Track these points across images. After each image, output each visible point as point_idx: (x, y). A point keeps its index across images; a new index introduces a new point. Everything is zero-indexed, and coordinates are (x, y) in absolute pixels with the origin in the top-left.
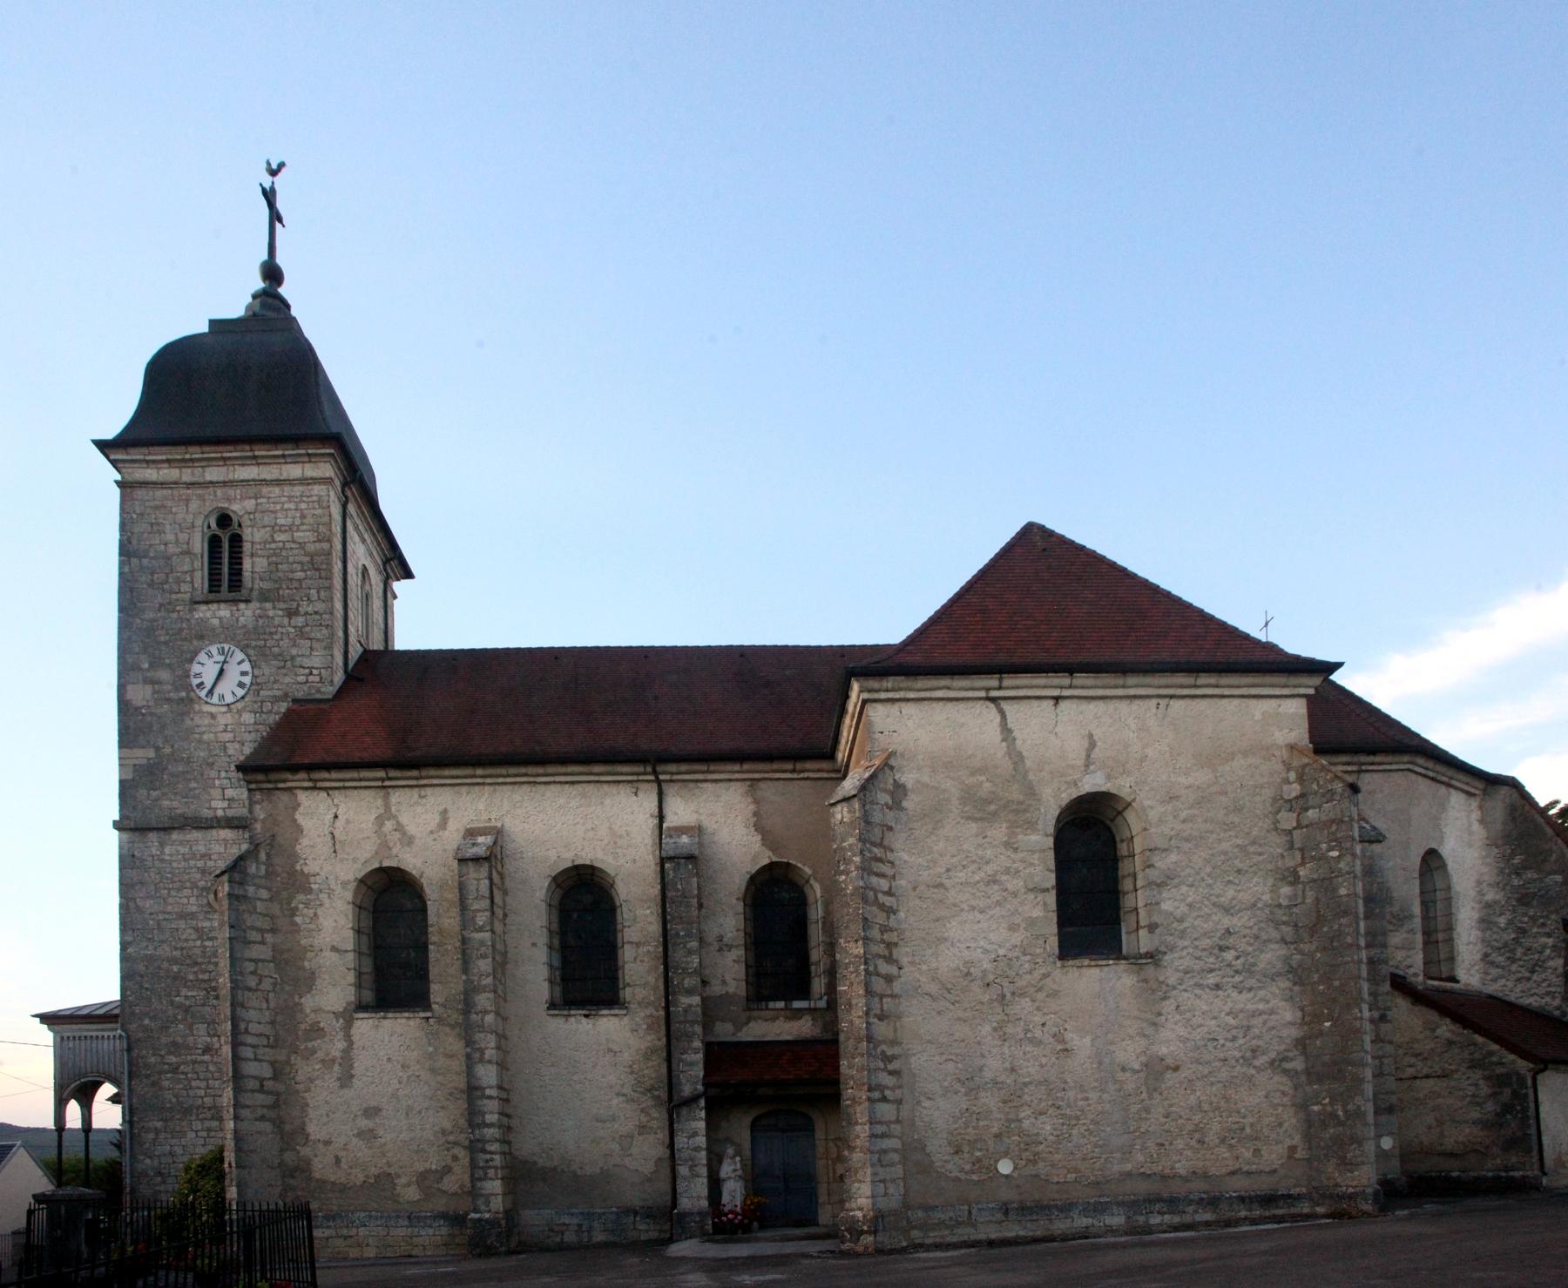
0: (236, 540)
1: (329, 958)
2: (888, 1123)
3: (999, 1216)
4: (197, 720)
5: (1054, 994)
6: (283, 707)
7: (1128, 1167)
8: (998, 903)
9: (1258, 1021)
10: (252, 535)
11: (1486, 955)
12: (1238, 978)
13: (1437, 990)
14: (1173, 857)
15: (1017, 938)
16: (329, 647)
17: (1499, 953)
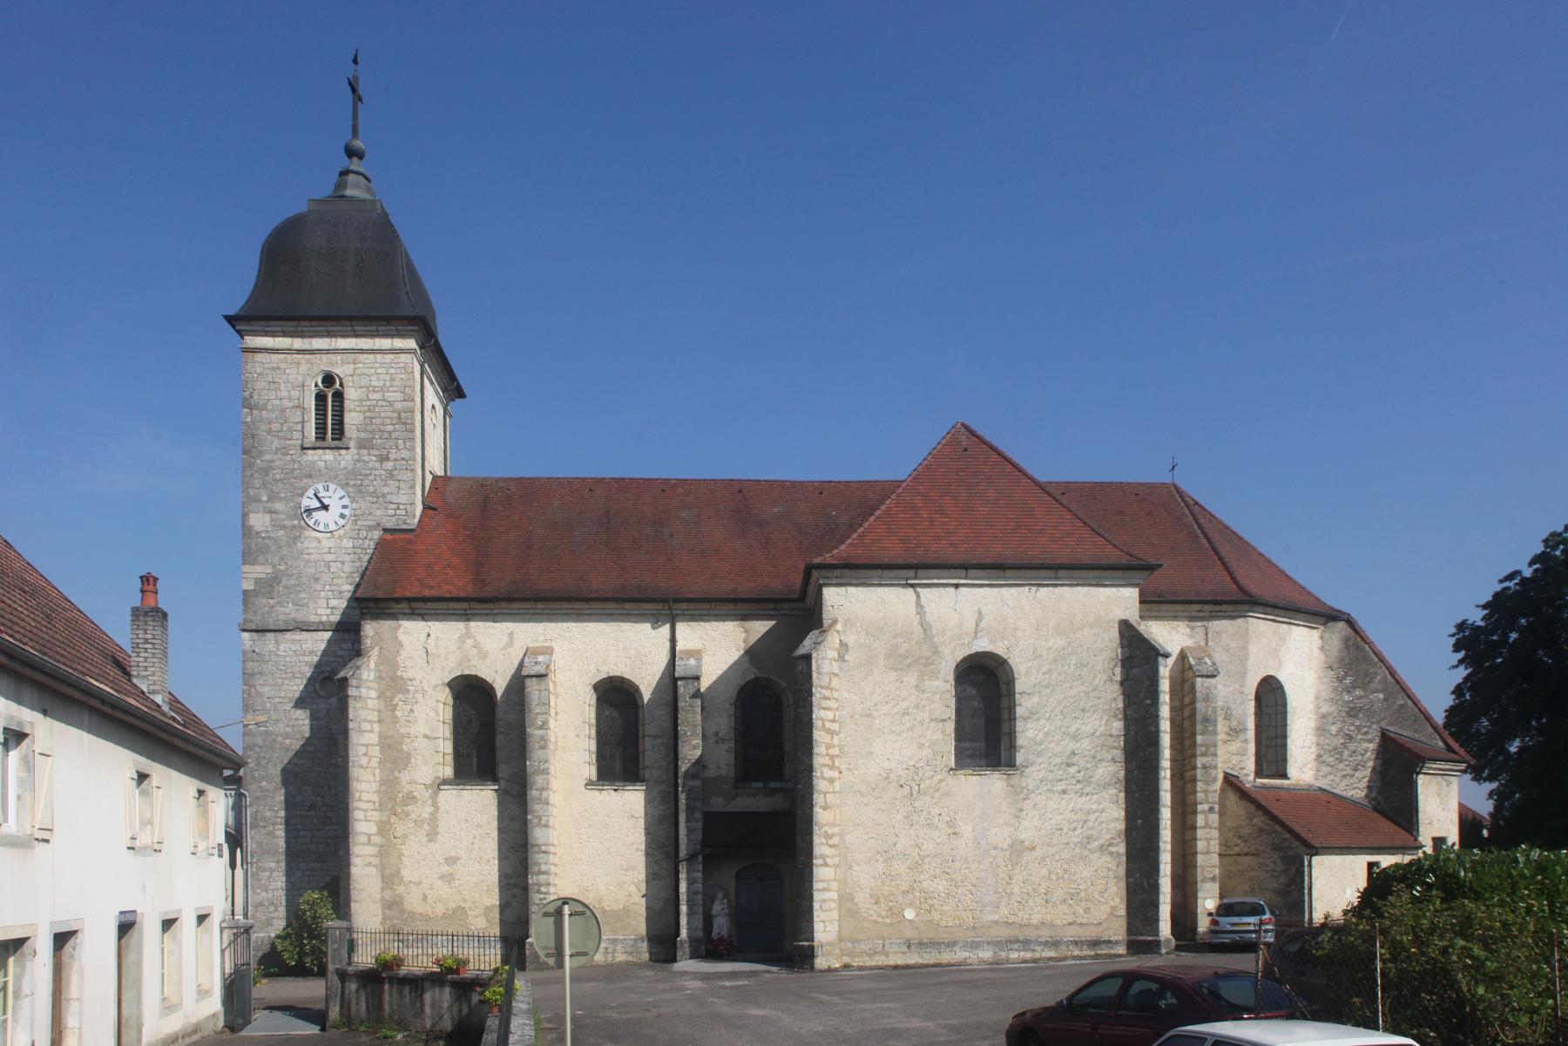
0: (339, 396)
1: (421, 743)
2: (828, 881)
3: (904, 948)
4: (307, 544)
5: (947, 794)
6: (377, 534)
7: (996, 917)
8: (910, 729)
9: (1092, 817)
10: (351, 395)
11: (1319, 756)
12: (1079, 786)
13: (1264, 787)
14: (1036, 699)
15: (926, 752)
16: (413, 487)
17: (1328, 754)
